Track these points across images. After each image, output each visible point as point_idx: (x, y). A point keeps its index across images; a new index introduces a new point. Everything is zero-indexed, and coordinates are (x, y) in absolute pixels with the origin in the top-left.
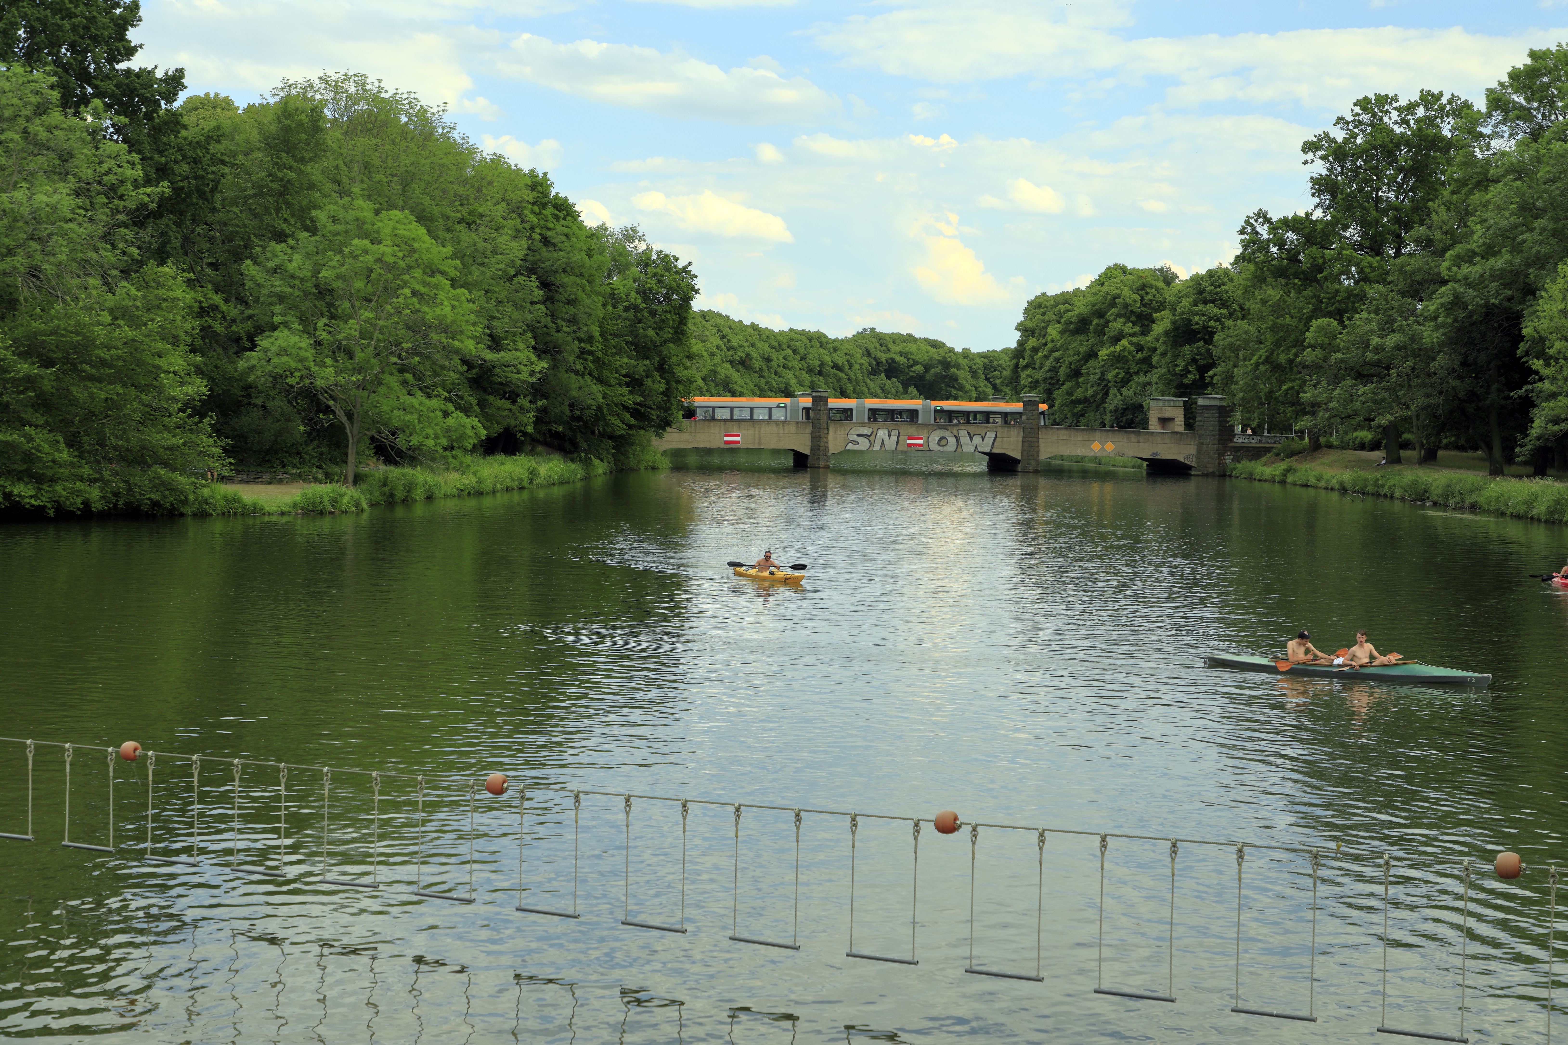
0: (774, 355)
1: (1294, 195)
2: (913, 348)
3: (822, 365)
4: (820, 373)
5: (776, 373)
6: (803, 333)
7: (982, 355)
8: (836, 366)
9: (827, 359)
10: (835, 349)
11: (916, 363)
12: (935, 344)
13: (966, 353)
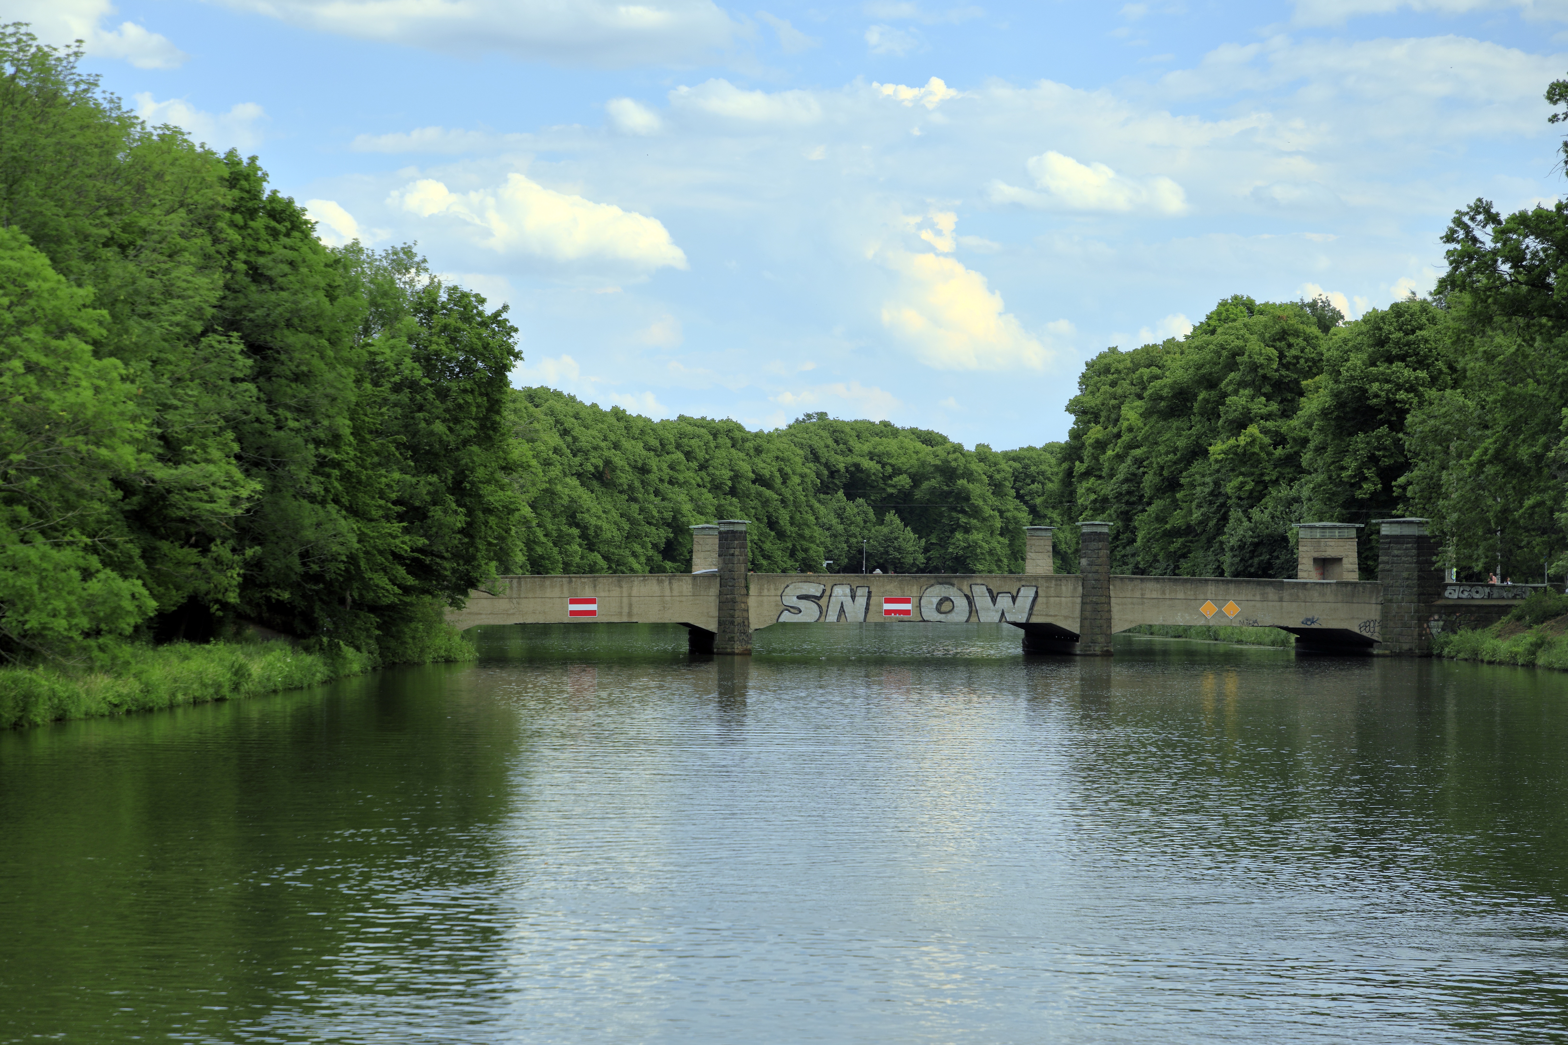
0: (653, 463)
1: (565, 393)
2: (891, 445)
3: (736, 477)
4: (733, 492)
5: (657, 493)
6: (702, 423)
7: (1011, 457)
8: (759, 480)
9: (745, 467)
10: (758, 451)
11: (897, 471)
12: (929, 439)
13: (983, 454)
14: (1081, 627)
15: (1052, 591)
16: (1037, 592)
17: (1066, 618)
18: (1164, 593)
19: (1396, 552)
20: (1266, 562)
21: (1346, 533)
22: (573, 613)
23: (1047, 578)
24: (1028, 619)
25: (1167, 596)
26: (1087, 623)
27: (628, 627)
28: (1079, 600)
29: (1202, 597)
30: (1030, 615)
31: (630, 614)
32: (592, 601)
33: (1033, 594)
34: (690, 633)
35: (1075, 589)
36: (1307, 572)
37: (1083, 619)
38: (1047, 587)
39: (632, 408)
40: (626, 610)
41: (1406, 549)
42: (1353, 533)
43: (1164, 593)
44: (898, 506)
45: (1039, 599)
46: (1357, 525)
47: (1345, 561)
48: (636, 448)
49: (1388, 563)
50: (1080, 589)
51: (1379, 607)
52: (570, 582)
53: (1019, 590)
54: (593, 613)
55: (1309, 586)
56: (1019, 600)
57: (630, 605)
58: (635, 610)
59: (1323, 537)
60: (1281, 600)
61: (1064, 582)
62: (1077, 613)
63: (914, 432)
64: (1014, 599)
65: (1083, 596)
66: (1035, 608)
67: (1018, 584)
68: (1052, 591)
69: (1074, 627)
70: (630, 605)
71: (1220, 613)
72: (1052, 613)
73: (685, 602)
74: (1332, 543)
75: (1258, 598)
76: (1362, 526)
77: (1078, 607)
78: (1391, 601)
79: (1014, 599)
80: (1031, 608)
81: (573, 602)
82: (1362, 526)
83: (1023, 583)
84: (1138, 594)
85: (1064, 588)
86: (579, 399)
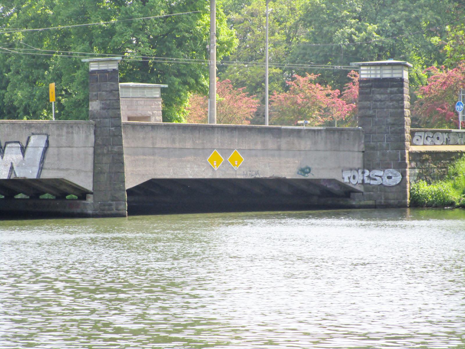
14: (94, 182)
15: (64, 140)
16: (47, 142)
17: (78, 171)
18: (174, 141)
19: (378, 97)
21: (147, 93)
24: (39, 174)
25: (177, 145)
26: (104, 178)
27: (213, 218)
28: (91, 150)
29: (209, 146)
30: (41, 169)
33: (43, 144)
35: (87, 137)
38: (59, 135)
41: (391, 93)
42: (157, 94)
43: (174, 141)
45: (50, 150)
46: (162, 86)
49: (369, 108)
50: (92, 137)
51: (361, 155)
53: (29, 138)
55: (303, 134)
56: (29, 150)
61: (76, 129)
62: (90, 166)
64: (23, 150)
65: (96, 146)
66: (46, 161)
67: (27, 132)
68: (64, 140)
69: (85, 182)
72: (64, 166)
75: (259, 147)
76: (166, 86)
77: (91, 158)
78: (373, 148)
79: (23, 150)
80: (42, 161)
82: (166, 86)
83: (33, 130)
84: (149, 144)
85: (75, 136)
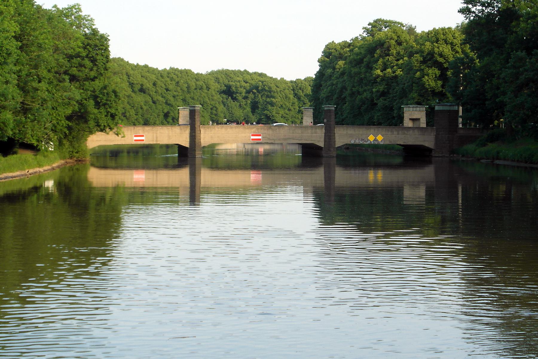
20: (393, 120)
22: (136, 140)
23: (311, 127)
31: (157, 141)
32: (143, 136)
34: (178, 147)
36: (407, 123)
37: (325, 141)
39: (152, 64)
40: (155, 139)
44: (246, 97)
47: (421, 119)
48: (153, 77)
52: (157, 173)
54: (143, 140)
57: (157, 138)
58: (158, 139)
59: (413, 111)
60: (398, 134)
63: (255, 73)
69: (322, 144)
70: (157, 138)
71: (375, 140)
73: (178, 136)
74: (416, 113)
81: (136, 136)
86: (150, 66)
